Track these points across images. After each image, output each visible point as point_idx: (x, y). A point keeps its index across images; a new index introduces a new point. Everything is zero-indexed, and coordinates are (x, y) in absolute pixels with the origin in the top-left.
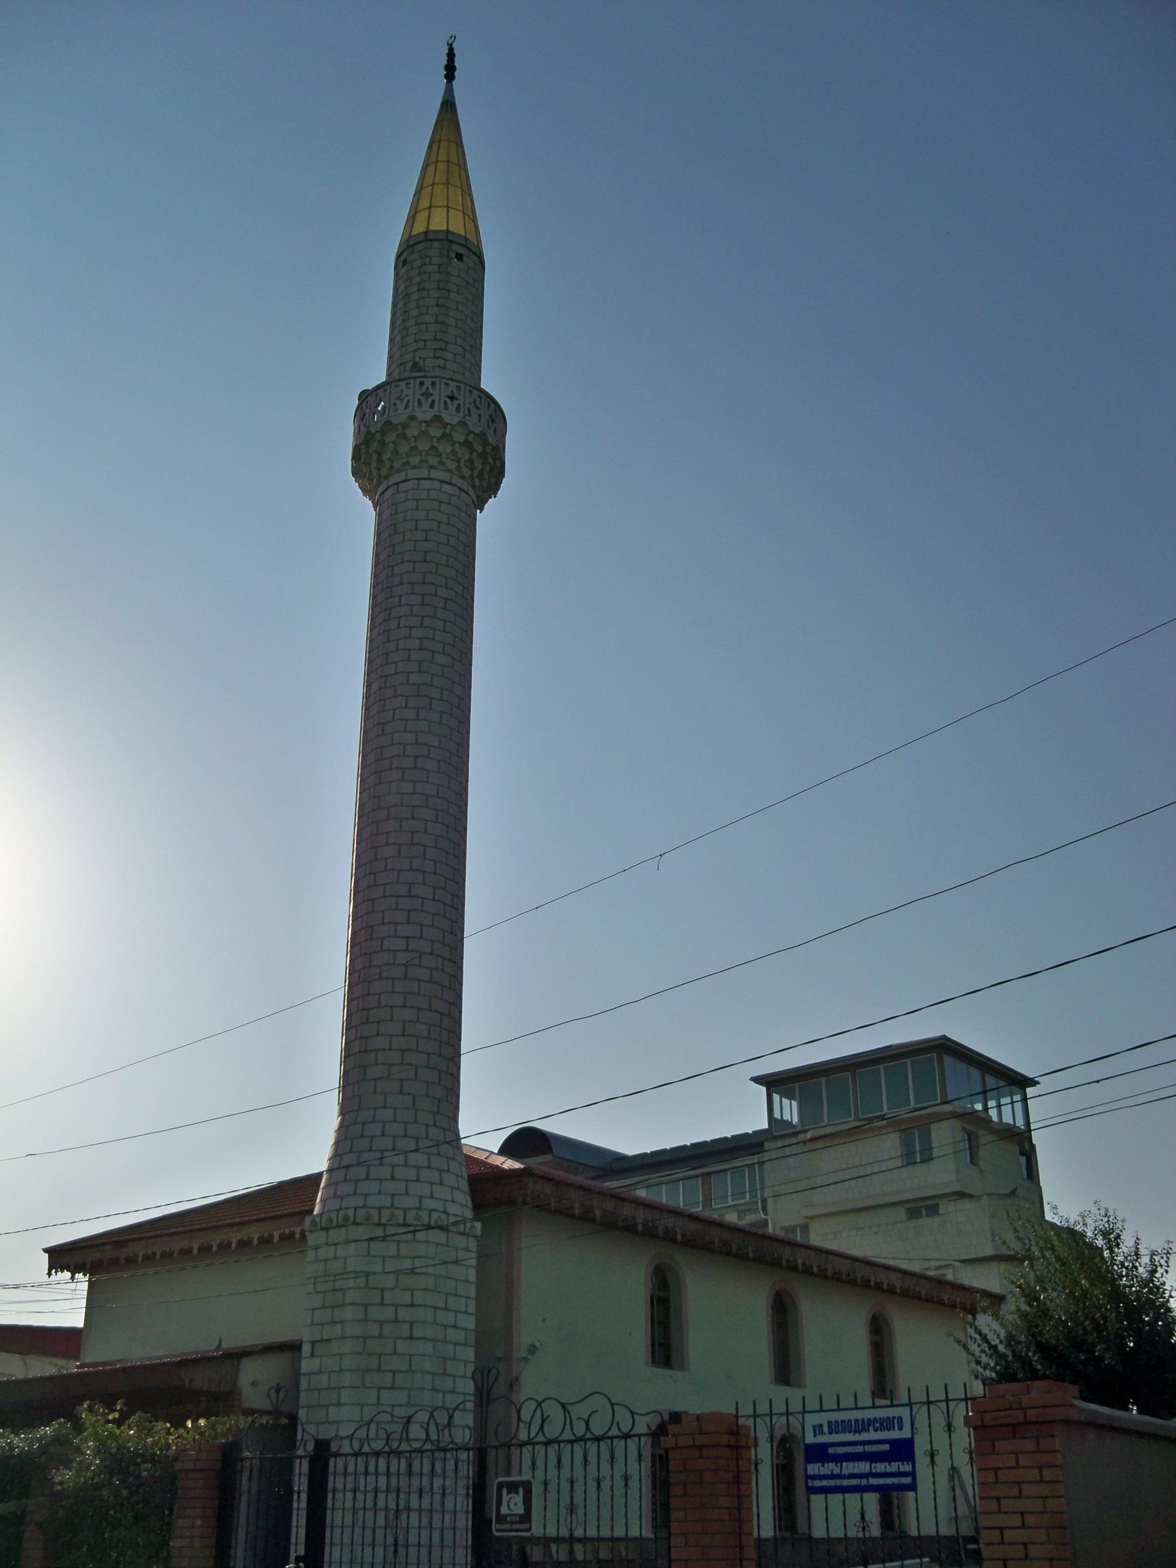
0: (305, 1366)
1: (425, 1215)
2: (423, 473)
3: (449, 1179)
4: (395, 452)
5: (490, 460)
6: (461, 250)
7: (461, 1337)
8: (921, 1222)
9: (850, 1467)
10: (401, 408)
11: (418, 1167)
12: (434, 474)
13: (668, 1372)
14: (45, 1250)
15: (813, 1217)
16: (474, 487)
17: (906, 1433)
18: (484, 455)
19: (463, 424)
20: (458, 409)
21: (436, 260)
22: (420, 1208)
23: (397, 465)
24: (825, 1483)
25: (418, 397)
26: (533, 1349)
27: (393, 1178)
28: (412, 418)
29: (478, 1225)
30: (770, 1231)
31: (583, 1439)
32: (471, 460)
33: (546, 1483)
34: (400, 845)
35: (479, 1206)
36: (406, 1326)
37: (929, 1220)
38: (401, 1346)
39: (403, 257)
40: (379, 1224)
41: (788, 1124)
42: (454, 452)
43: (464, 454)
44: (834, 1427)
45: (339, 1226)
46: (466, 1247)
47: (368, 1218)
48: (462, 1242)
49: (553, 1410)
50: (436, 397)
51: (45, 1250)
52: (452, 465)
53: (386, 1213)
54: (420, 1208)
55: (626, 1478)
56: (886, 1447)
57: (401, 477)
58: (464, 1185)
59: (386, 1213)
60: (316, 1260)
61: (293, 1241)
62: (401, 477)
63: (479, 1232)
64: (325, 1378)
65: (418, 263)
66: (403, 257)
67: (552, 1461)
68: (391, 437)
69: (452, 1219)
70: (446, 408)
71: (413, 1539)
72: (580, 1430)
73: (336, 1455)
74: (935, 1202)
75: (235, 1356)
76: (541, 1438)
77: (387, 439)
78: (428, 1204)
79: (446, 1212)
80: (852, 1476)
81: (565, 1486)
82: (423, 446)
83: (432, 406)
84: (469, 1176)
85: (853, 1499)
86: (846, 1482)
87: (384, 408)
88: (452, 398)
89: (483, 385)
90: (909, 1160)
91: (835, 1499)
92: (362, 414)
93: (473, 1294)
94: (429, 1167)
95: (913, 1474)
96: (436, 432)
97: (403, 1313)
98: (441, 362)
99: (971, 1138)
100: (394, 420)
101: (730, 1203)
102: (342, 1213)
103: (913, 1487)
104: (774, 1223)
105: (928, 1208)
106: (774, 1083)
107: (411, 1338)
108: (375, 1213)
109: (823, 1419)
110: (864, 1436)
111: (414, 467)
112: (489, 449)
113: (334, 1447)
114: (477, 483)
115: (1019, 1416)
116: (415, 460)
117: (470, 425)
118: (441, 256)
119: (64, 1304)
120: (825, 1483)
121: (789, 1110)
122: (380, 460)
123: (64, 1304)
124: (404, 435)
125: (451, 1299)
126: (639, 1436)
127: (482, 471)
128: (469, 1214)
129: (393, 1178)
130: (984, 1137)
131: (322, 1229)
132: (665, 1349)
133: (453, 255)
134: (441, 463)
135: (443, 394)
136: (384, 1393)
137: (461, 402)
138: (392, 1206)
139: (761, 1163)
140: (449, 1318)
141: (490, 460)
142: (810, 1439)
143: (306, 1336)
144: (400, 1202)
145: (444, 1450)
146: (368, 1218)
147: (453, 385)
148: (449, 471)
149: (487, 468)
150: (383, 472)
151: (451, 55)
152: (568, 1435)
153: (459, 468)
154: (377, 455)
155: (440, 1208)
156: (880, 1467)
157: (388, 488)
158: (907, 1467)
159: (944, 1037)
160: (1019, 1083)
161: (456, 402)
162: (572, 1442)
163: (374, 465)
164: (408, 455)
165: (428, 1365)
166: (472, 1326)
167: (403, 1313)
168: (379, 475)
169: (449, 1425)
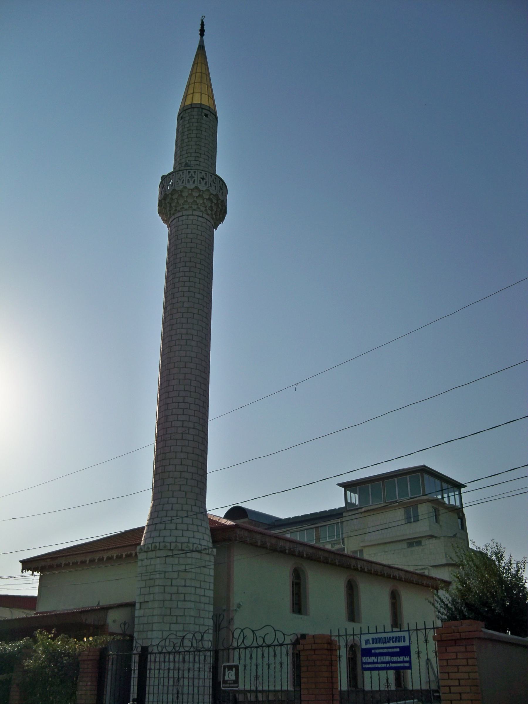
0: (137, 613)
1: (191, 545)
2: (190, 212)
4: (178, 203)
5: (220, 206)
6: (207, 112)
7: (207, 600)
8: (413, 549)
9: (382, 659)
11: (188, 524)
12: (195, 213)
13: (300, 616)
14: (20, 561)
15: (365, 547)
16: (213, 219)
17: (407, 644)
18: (217, 204)
19: (208, 190)
20: (206, 184)
23: (178, 209)
24: (370, 666)
25: (188, 178)
26: (239, 606)
27: (176, 529)
28: (185, 188)
29: (215, 550)
31: (261, 646)
32: (211, 207)
33: (245, 666)
34: (180, 379)
35: (215, 541)
37: (417, 548)
40: (170, 550)
41: (354, 505)
42: (204, 203)
44: (374, 641)
45: (152, 551)
46: (209, 560)
47: (165, 547)
48: (207, 558)
50: (196, 178)
51: (20, 561)
52: (203, 209)
53: (173, 545)
54: (188, 542)
55: (281, 664)
56: (398, 650)
57: (180, 214)
58: (208, 532)
59: (173, 545)
60: (142, 566)
61: (131, 557)
62: (180, 214)
63: (215, 553)
64: (146, 618)
65: (187, 118)
67: (248, 656)
68: (175, 196)
69: (203, 547)
70: (200, 183)
71: (185, 691)
72: (260, 642)
73: (151, 653)
74: (420, 540)
75: (106, 609)
76: (243, 646)
77: (174, 197)
78: (192, 540)
79: (200, 544)
80: (383, 663)
81: (254, 667)
82: (190, 200)
84: (210, 528)
85: (383, 673)
86: (380, 666)
87: (172, 183)
88: (203, 179)
90: (408, 521)
91: (375, 673)
92: (162, 186)
93: (212, 581)
94: (193, 524)
95: (410, 662)
96: (196, 194)
97: (181, 590)
98: (198, 163)
99: (436, 511)
101: (328, 540)
102: (153, 545)
103: (410, 668)
104: (347, 549)
105: (417, 542)
106: (348, 486)
107: (185, 601)
109: (370, 637)
110: (388, 645)
111: (186, 210)
112: (219, 201)
113: (150, 650)
114: (214, 217)
115: (458, 636)
116: (186, 207)
117: (211, 191)
118: (198, 115)
119: (29, 586)
120: (370, 666)
121: (354, 498)
122: (171, 206)
123: (29, 586)
125: (202, 583)
126: (287, 645)
127: (216, 211)
128: (211, 545)
129: (176, 529)
130: (442, 511)
131: (145, 552)
132: (298, 605)
133: (203, 115)
134: (198, 208)
136: (172, 625)
137: (207, 180)
138: (176, 542)
139: (342, 522)
140: (202, 592)
141: (220, 206)
142: (364, 646)
143: (138, 600)
145: (200, 651)
146: (165, 547)
147: (203, 173)
148: (202, 211)
149: (219, 210)
150: (172, 212)
151: (202, 25)
152: (255, 644)
153: (206, 210)
154: (169, 204)
155: (198, 542)
156: (395, 659)
157: (174, 219)
158: (407, 659)
159: (424, 466)
160: (458, 486)
162: (257, 647)
164: (183, 204)
166: (212, 595)
167: (181, 590)
169: (202, 640)
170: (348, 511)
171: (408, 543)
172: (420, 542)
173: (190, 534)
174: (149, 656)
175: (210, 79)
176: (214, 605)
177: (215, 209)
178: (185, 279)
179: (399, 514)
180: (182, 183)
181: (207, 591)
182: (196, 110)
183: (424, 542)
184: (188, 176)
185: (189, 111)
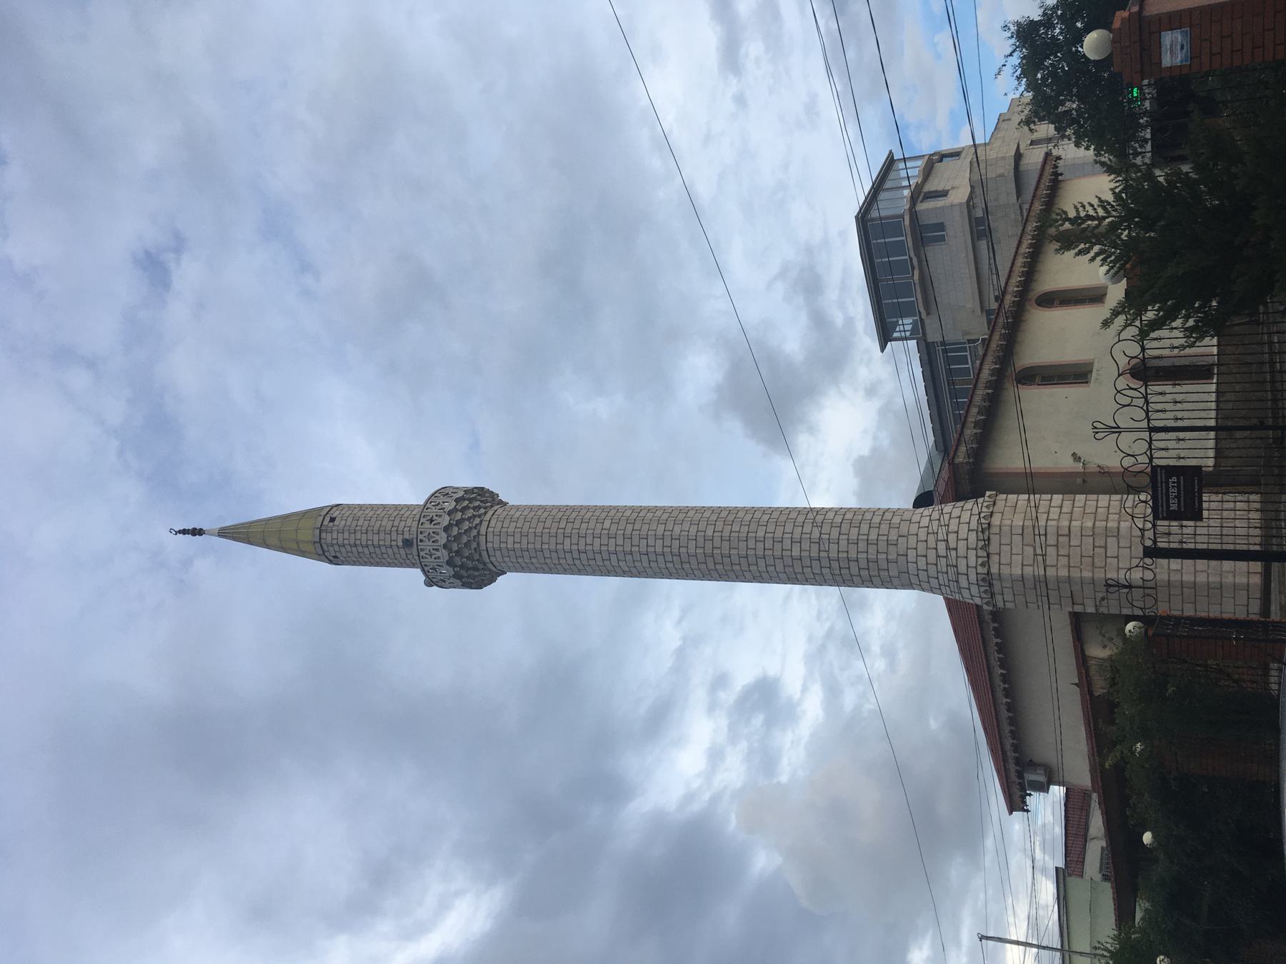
0: (1091, 610)
3: (956, 512)
6: (328, 519)
7: (1067, 504)
10: (438, 554)
12: (483, 531)
14: (1011, 813)
18: (471, 500)
23: (476, 557)
26: (1076, 457)
29: (988, 493)
32: (474, 508)
35: (976, 494)
36: (1061, 539)
41: (915, 323)
43: (470, 513)
45: (991, 585)
47: (983, 565)
48: (1000, 504)
51: (1011, 813)
52: (477, 521)
58: (960, 504)
62: (484, 554)
73: (1155, 542)
75: (1082, 660)
78: (974, 525)
89: (422, 502)
90: (942, 239)
92: (441, 584)
96: (455, 531)
100: (447, 558)
107: (1069, 535)
108: (980, 560)
113: (1149, 543)
119: (1048, 806)
123: (1048, 806)
130: (927, 188)
132: (1077, 374)
139: (943, 343)
146: (983, 565)
150: (481, 566)
153: (479, 516)
159: (857, 217)
160: (890, 162)
170: (924, 334)
173: (964, 528)
174: (1160, 545)
176: (1075, 492)
179: (936, 254)
184: (429, 560)
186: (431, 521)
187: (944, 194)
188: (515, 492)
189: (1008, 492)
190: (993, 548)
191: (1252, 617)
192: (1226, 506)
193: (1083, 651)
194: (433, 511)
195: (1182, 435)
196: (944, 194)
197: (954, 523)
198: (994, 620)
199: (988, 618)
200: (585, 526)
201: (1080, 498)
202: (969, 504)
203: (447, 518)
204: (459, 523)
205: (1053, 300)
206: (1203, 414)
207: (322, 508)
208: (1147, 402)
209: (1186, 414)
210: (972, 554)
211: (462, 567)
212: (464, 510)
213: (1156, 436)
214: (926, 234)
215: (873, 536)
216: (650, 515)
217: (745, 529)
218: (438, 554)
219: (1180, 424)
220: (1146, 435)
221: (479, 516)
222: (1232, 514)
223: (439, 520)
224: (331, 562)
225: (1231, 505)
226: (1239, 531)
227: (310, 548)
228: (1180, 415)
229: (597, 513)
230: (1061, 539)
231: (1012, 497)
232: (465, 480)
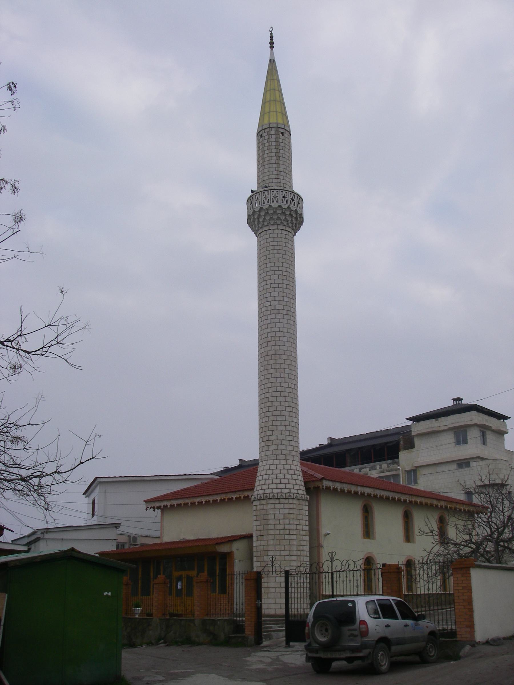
0: (255, 544)
1: (292, 495)
3: (298, 482)
4: (265, 219)
5: (299, 219)
6: (282, 131)
7: (304, 533)
8: (462, 470)
10: (266, 202)
12: (279, 227)
13: (369, 540)
16: (293, 230)
19: (289, 208)
21: (274, 136)
22: (290, 493)
23: (266, 224)
25: (272, 198)
28: (270, 206)
30: (401, 484)
33: (350, 581)
34: (276, 369)
37: (466, 469)
38: (287, 537)
39: (261, 133)
40: (277, 498)
42: (286, 218)
45: (264, 499)
47: (274, 496)
48: (303, 503)
49: (351, 562)
50: (278, 198)
51: (145, 501)
53: (279, 495)
54: (290, 493)
57: (267, 228)
58: (303, 484)
59: (279, 495)
62: (267, 228)
64: (262, 547)
65: (267, 137)
66: (261, 133)
67: (352, 575)
68: (263, 213)
70: (283, 202)
73: (291, 574)
76: (348, 570)
78: (292, 491)
79: (298, 493)
81: (355, 582)
82: (275, 217)
83: (277, 202)
88: (284, 197)
90: (458, 443)
96: (279, 212)
97: (287, 527)
98: (279, 180)
99: (484, 435)
102: (265, 495)
105: (465, 463)
107: (289, 534)
108: (276, 495)
114: (294, 228)
116: (272, 222)
117: (291, 207)
122: (259, 221)
124: (268, 212)
125: (301, 521)
127: (296, 224)
128: (305, 493)
132: (368, 532)
134: (281, 222)
135: (281, 196)
144: (283, 491)
146: (274, 496)
147: (284, 192)
148: (285, 225)
150: (260, 226)
151: (272, 37)
152: (355, 569)
153: (288, 224)
161: (286, 199)
163: (256, 223)
164: (269, 220)
165: (295, 543)
167: (287, 527)
168: (259, 227)
171: (457, 464)
172: (469, 463)
173: (291, 486)
175: (284, 106)
177: (294, 222)
178: (276, 285)
180: (268, 202)
181: (304, 527)
182: (273, 129)
183: (473, 464)
185: (267, 130)
186: (284, 197)
187: (484, 443)
188: (302, 242)
189: (309, 506)
190: (282, 501)
191: (263, 610)
192: (305, 600)
193: (235, 540)
194: (289, 198)
195: (330, 583)
196: (484, 443)
197: (293, 482)
198: (244, 497)
199: (246, 494)
200: (284, 261)
201: (307, 538)
202: (303, 488)
203: (286, 207)
204: (283, 213)
205: (407, 517)
206: (348, 589)
207: (289, 127)
208: (343, 571)
209: (338, 585)
210: (287, 491)
211: (259, 216)
212: (291, 215)
213: (330, 574)
214: (461, 435)
215: (284, 442)
216: (292, 323)
217: (286, 376)
218: (266, 202)
219: (335, 583)
220: (330, 571)
221: (288, 224)
222: (302, 602)
223: (285, 202)
224: (258, 133)
225: (305, 602)
226: (302, 591)
227: (266, 121)
228: (338, 582)
229: (288, 183)
230: (288, 531)
231: (307, 508)
232: (308, 212)
